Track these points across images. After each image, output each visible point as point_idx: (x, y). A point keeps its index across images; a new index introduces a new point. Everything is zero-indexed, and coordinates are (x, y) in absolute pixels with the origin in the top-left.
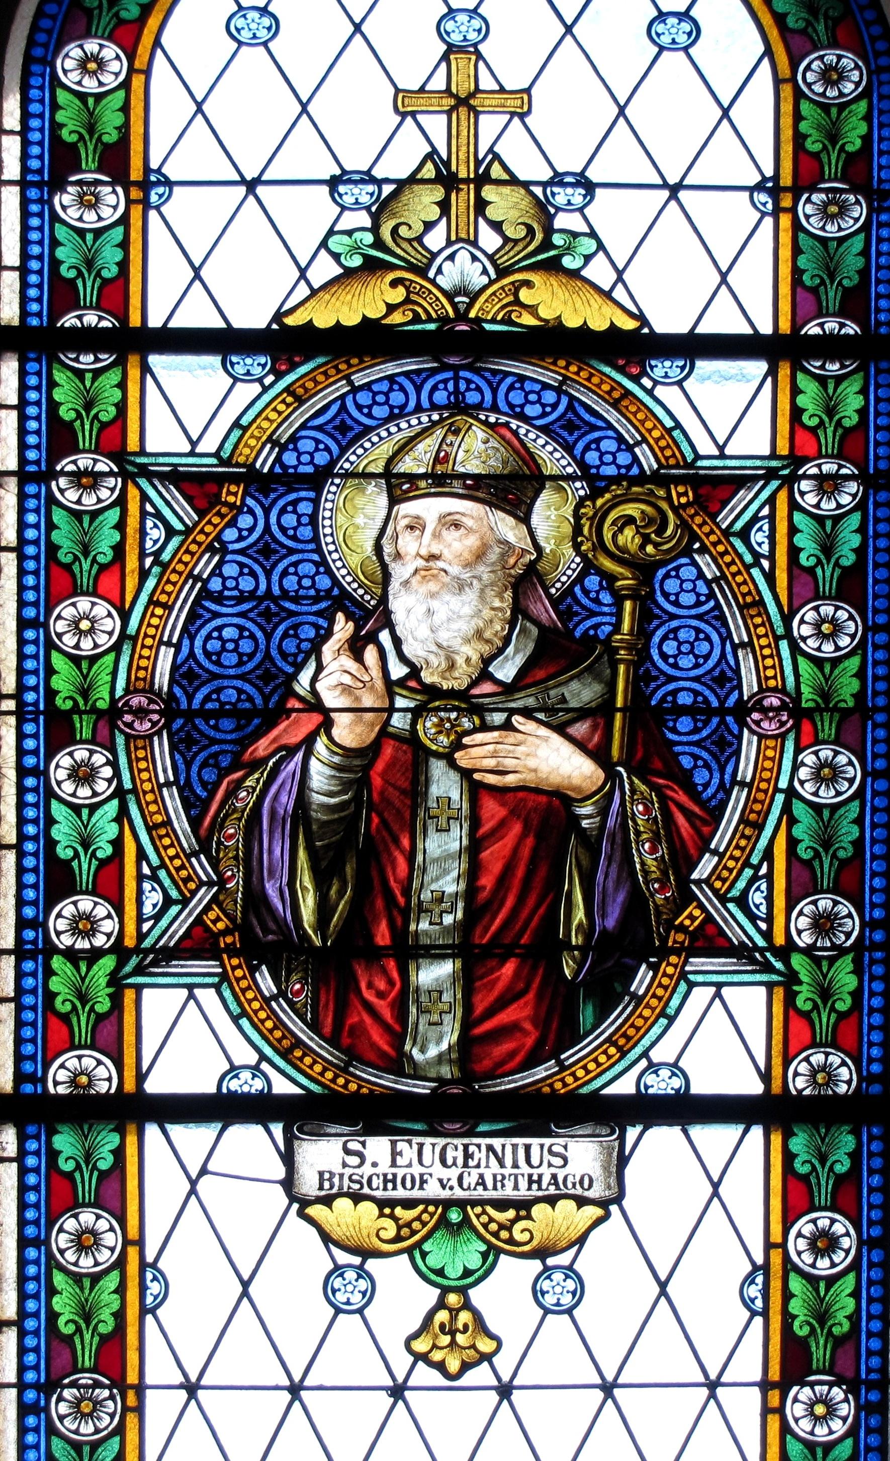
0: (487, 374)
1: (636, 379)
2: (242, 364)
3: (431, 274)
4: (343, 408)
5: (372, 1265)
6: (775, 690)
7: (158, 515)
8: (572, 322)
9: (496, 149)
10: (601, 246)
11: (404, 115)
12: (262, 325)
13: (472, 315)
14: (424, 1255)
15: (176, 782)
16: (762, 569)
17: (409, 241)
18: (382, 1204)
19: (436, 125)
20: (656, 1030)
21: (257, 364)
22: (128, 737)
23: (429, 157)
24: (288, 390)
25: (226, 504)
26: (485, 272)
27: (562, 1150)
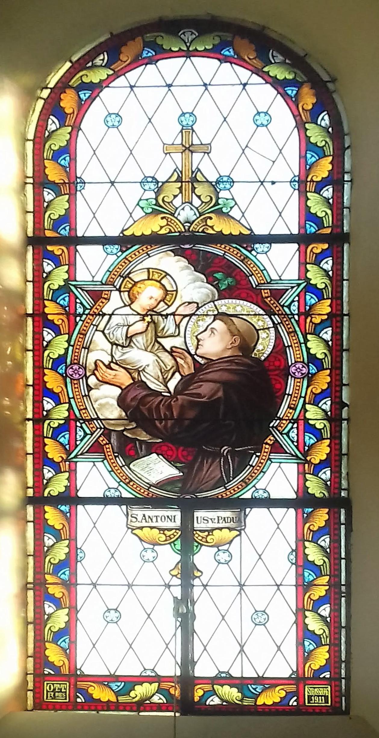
1: (250, 252)
2: (109, 248)
3: (176, 215)
5: (156, 548)
8: (226, 232)
9: (199, 167)
10: (236, 204)
11: (166, 154)
14: (175, 545)
16: (295, 320)
17: (168, 203)
19: (178, 157)
20: (266, 274)
21: (115, 248)
22: (71, 379)
23: (175, 170)
26: (195, 214)
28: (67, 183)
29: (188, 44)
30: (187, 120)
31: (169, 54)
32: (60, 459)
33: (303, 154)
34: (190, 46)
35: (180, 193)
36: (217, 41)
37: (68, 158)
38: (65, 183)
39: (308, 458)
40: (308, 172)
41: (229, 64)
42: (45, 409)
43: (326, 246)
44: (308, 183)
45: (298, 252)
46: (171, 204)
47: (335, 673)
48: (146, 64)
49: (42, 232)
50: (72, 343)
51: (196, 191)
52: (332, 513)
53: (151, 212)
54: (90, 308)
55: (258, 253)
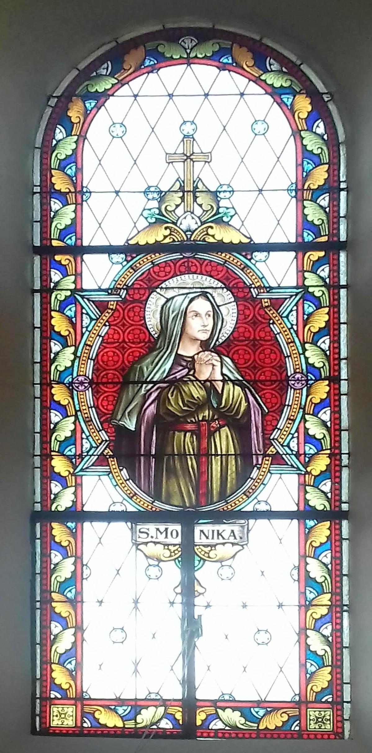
0: (199, 260)
1: (250, 260)
4: (149, 273)
5: (161, 564)
6: (299, 373)
7: (87, 314)
8: (226, 240)
10: (236, 213)
11: (169, 163)
12: (122, 244)
13: (192, 239)
15: (94, 407)
17: (171, 212)
18: (165, 545)
23: (177, 180)
24: (131, 267)
25: (110, 309)
26: (196, 223)
27: (146, 531)
28: (73, 192)
29: (188, 51)
30: (188, 129)
31: (170, 61)
32: (67, 473)
33: (300, 161)
34: (190, 52)
35: (182, 202)
36: (217, 48)
37: (74, 168)
38: (70, 192)
39: (309, 469)
40: (305, 180)
41: (227, 71)
42: (53, 493)
43: (322, 254)
44: (305, 192)
45: (295, 260)
46: (173, 212)
47: (337, 696)
48: (148, 73)
49: (49, 241)
50: (79, 354)
51: (198, 200)
52: (332, 384)
53: (155, 223)
54: (95, 318)
55: (257, 261)
